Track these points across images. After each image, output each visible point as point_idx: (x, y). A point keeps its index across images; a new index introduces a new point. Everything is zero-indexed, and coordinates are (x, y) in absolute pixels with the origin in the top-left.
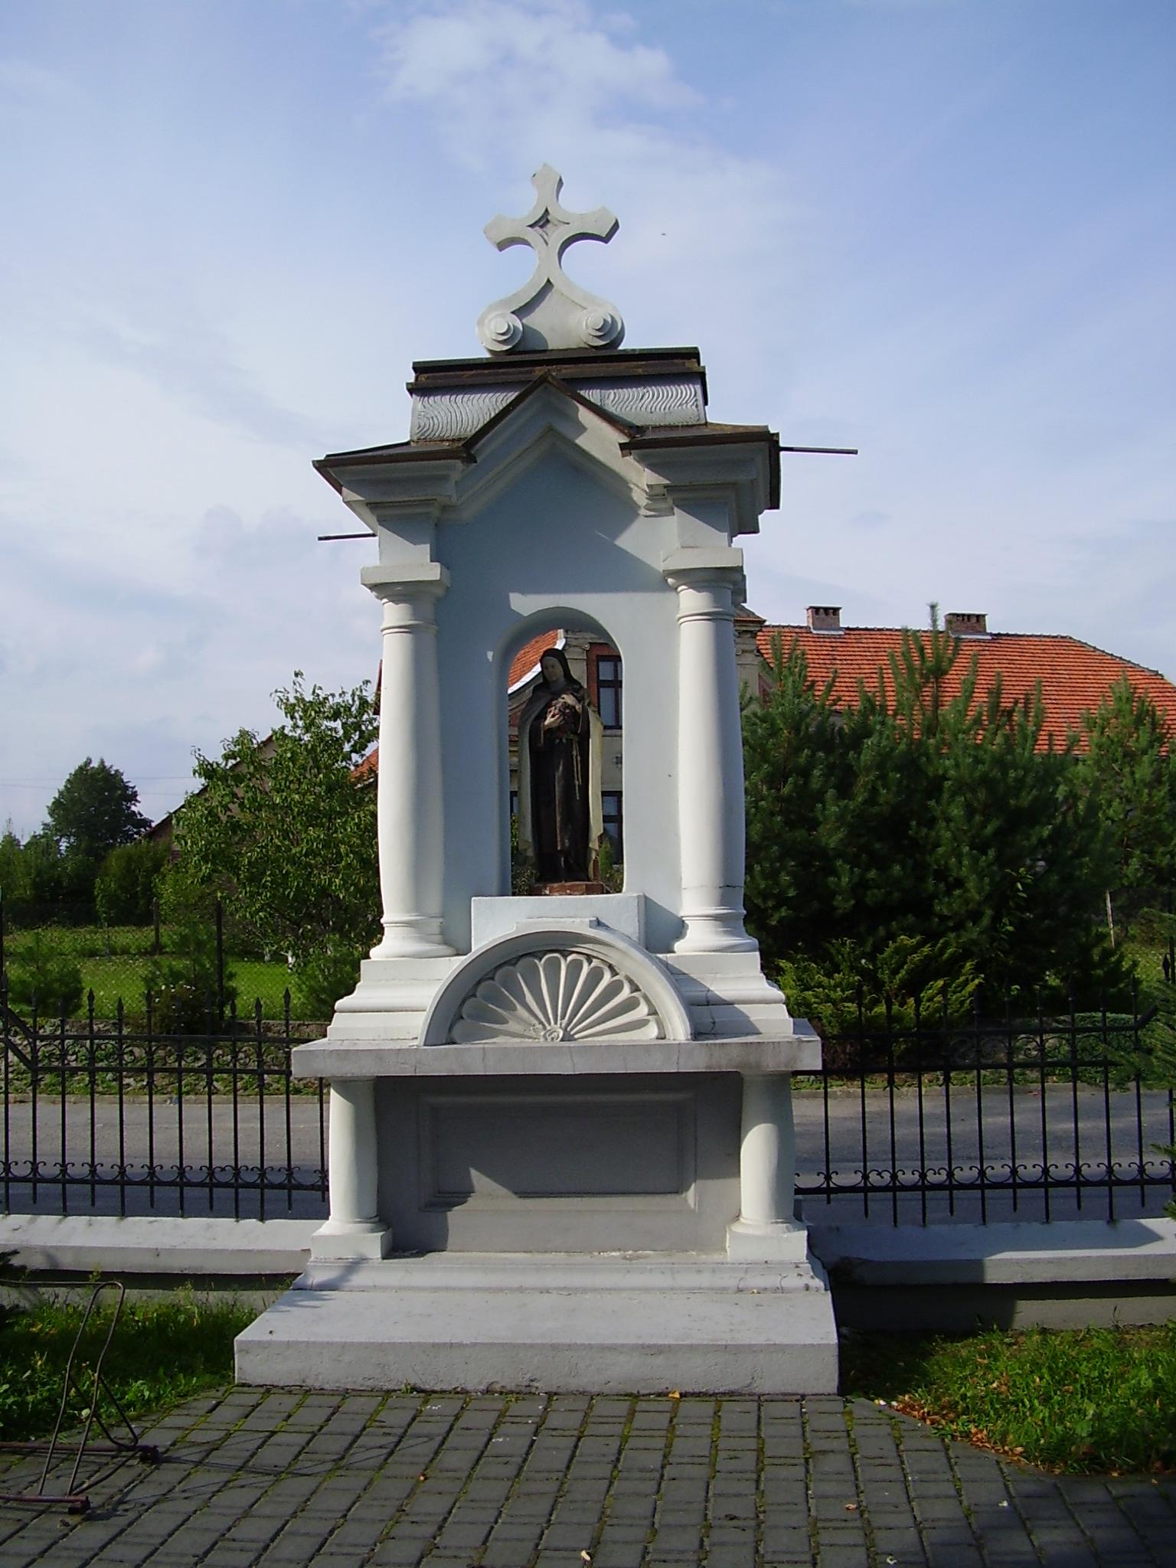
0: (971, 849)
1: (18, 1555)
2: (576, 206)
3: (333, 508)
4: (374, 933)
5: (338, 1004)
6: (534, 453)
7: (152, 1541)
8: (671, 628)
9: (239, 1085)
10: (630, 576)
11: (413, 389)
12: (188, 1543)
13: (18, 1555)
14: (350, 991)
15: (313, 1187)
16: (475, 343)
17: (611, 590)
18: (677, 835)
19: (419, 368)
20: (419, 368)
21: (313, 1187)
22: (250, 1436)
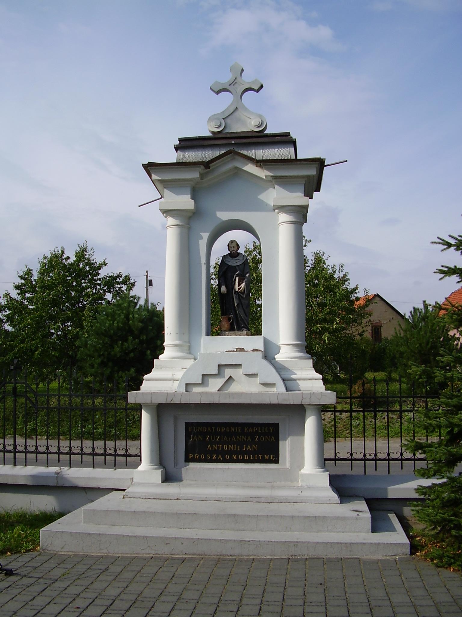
0: (125, 317)
1: (132, 571)
2: (248, 79)
3: (146, 188)
4: (162, 349)
5: (145, 377)
6: (218, 162)
7: (137, 592)
8: (275, 228)
9: (386, 419)
10: (261, 207)
11: (177, 148)
12: (54, 609)
13: (132, 571)
14: (150, 372)
15: (136, 456)
16: (204, 130)
17: (242, 211)
18: (279, 326)
19: (181, 140)
20: (181, 140)
21: (136, 456)
22: (29, 568)
